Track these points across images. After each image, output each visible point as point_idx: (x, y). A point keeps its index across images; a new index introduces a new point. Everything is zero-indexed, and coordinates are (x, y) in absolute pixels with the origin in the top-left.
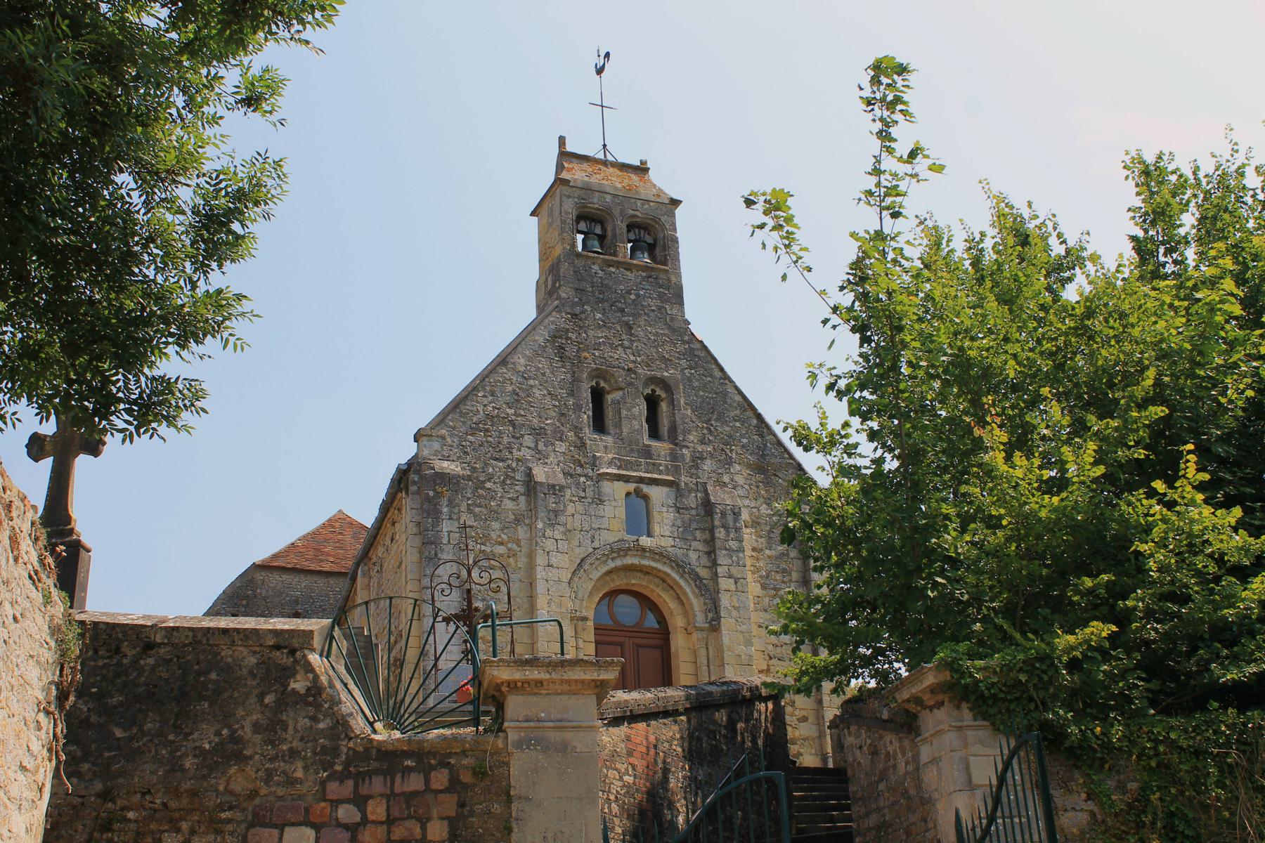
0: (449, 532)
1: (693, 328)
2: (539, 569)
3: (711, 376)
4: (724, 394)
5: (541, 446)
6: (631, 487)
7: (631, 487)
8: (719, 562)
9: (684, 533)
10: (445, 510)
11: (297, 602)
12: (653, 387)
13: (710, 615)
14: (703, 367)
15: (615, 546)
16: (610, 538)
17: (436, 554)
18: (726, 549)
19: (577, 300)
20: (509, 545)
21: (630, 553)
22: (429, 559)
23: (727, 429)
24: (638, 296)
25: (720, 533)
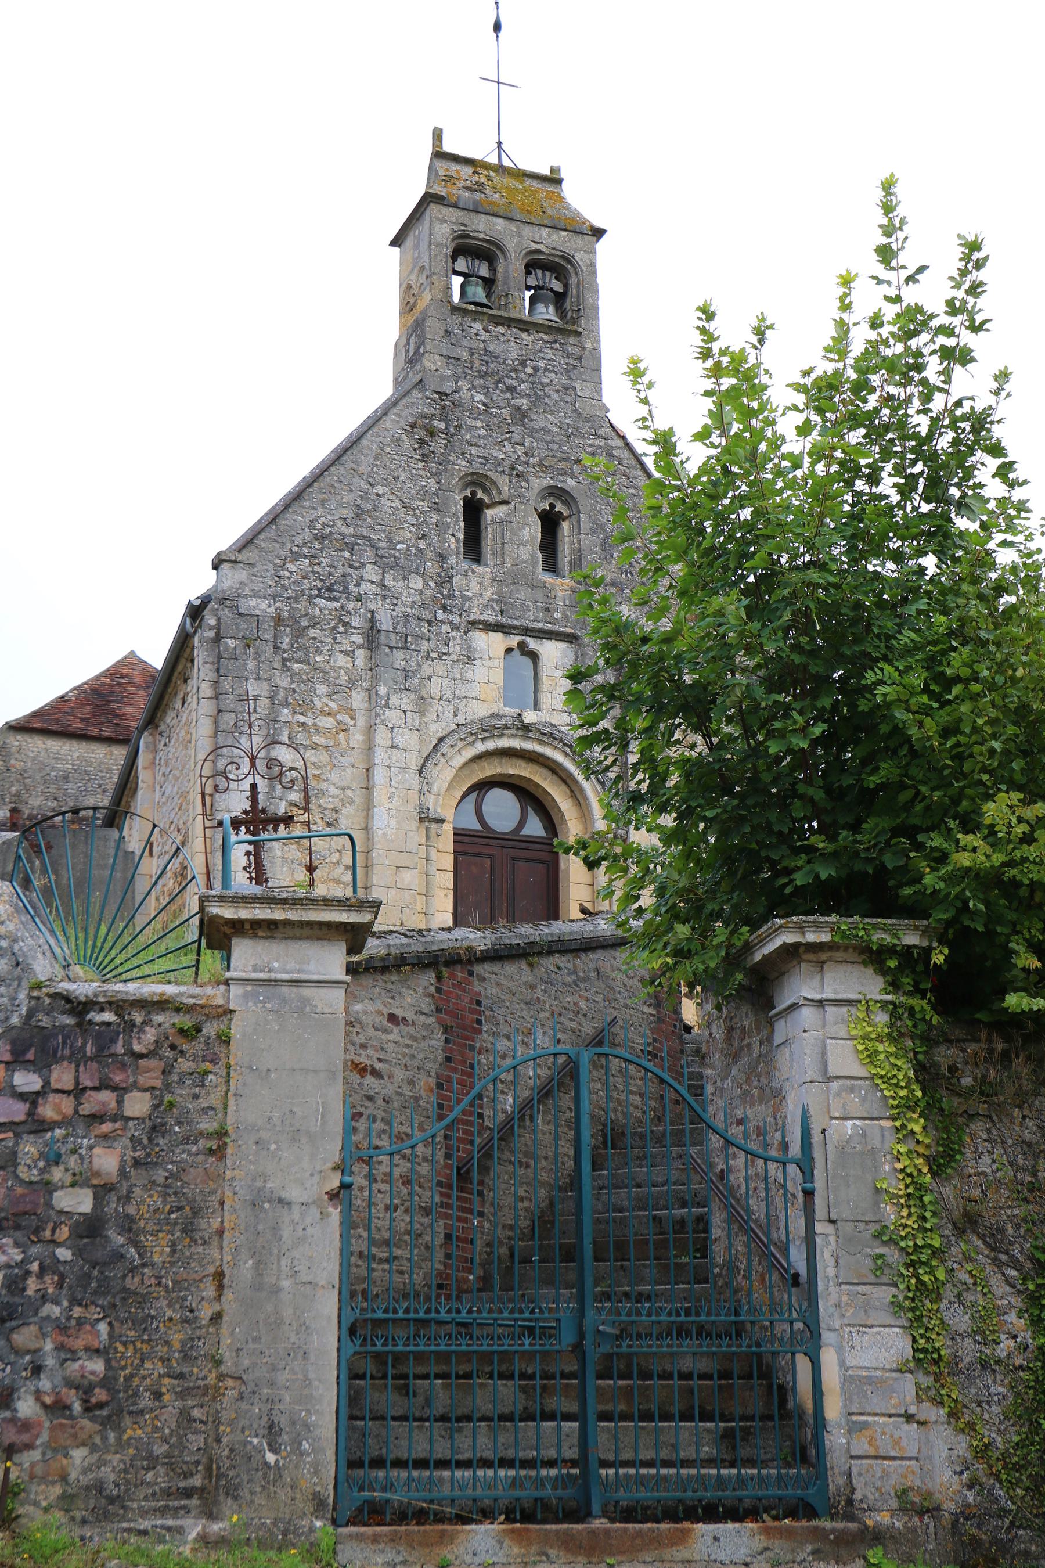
5: (389, 581)
6: (514, 640)
7: (514, 640)
11: (66, 779)
16: (479, 711)
21: (506, 732)
24: (536, 369)
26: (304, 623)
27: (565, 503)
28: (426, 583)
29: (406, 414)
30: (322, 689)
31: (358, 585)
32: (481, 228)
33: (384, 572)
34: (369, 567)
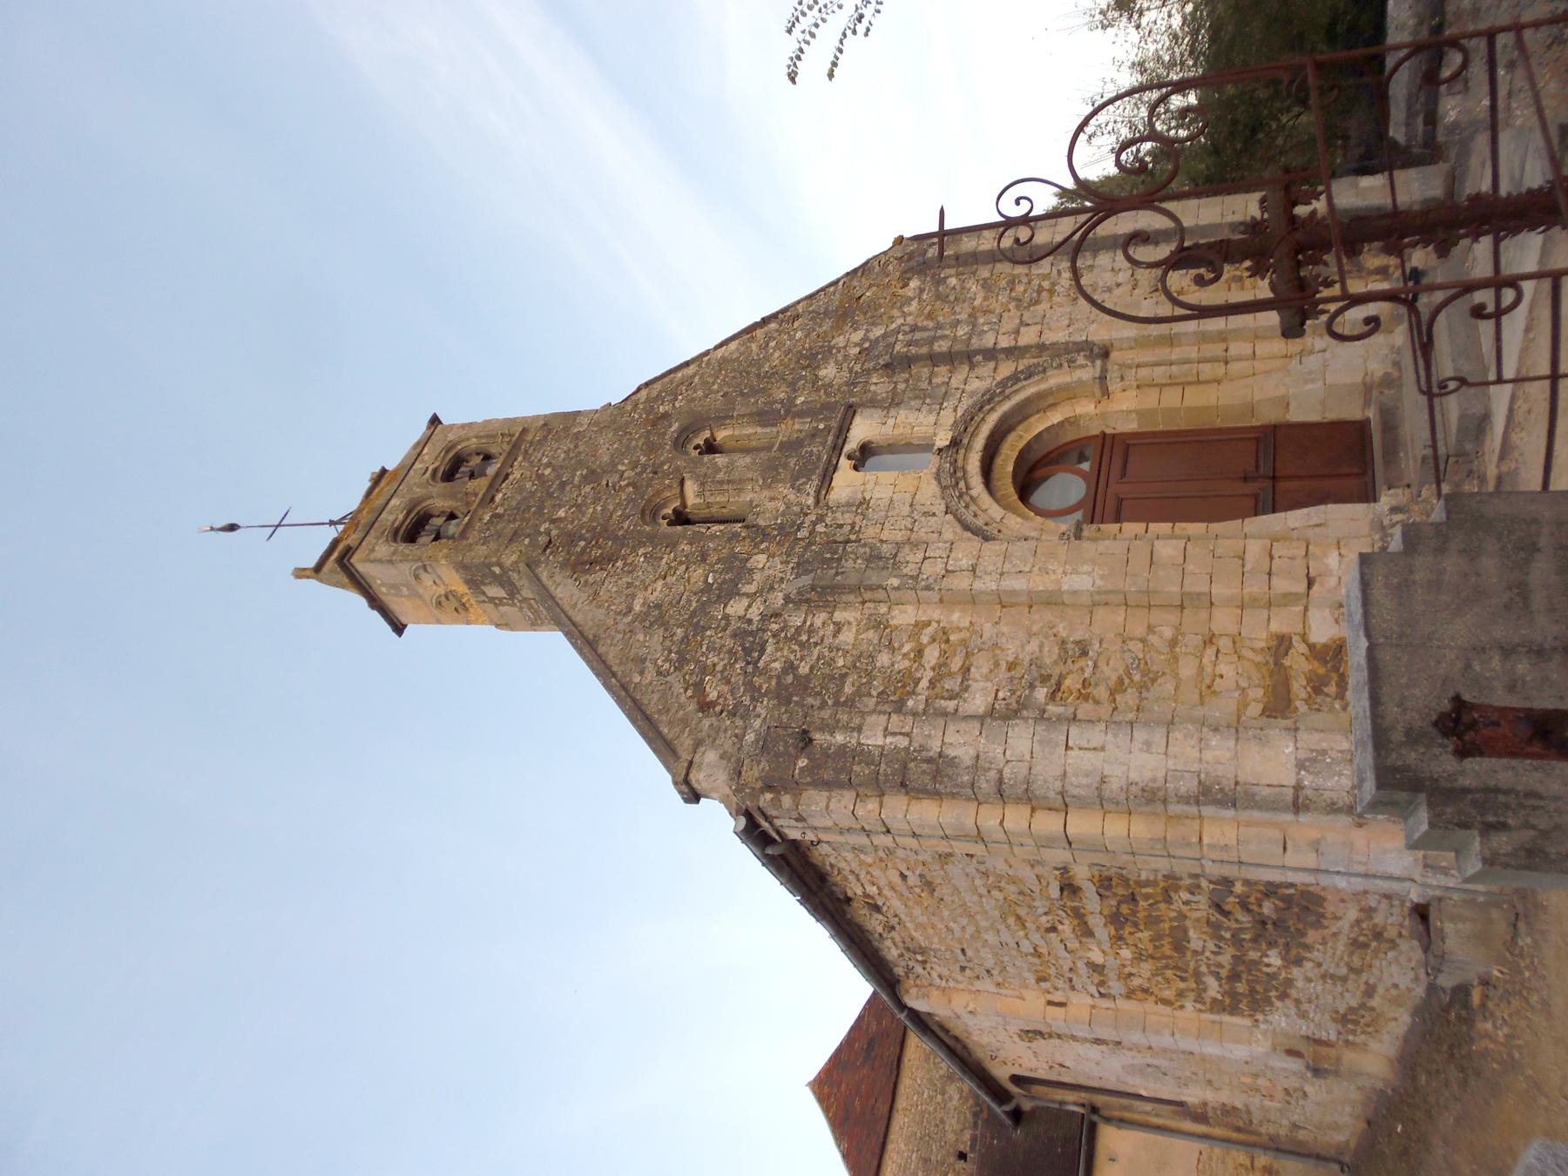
0: (887, 732)
1: (616, 399)
2: (978, 585)
3: (694, 376)
4: (724, 361)
5: (751, 589)
6: (844, 463)
7: (844, 463)
8: (990, 344)
9: (934, 398)
10: (840, 738)
11: (926, 1161)
12: (690, 448)
13: (1081, 360)
14: (677, 386)
15: (947, 481)
16: (929, 491)
17: (929, 761)
18: (970, 339)
19: (527, 541)
20: (925, 639)
21: (960, 463)
22: (937, 775)
23: (777, 354)
24: (549, 465)
25: (941, 346)
26: (790, 679)
27: (696, 432)
28: (763, 552)
29: (566, 590)
30: (884, 659)
31: (750, 621)
32: (392, 518)
33: (738, 594)
34: (729, 610)
